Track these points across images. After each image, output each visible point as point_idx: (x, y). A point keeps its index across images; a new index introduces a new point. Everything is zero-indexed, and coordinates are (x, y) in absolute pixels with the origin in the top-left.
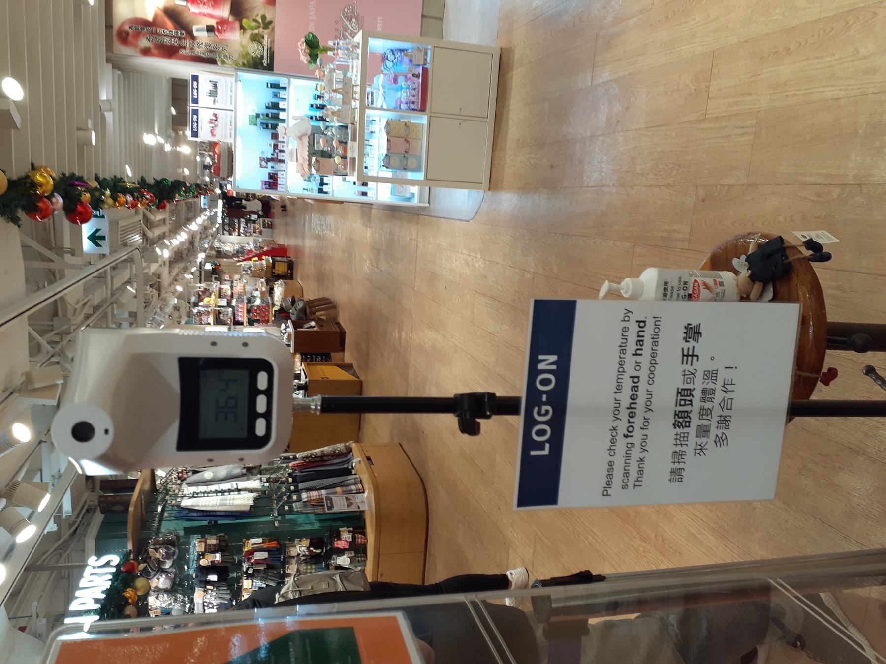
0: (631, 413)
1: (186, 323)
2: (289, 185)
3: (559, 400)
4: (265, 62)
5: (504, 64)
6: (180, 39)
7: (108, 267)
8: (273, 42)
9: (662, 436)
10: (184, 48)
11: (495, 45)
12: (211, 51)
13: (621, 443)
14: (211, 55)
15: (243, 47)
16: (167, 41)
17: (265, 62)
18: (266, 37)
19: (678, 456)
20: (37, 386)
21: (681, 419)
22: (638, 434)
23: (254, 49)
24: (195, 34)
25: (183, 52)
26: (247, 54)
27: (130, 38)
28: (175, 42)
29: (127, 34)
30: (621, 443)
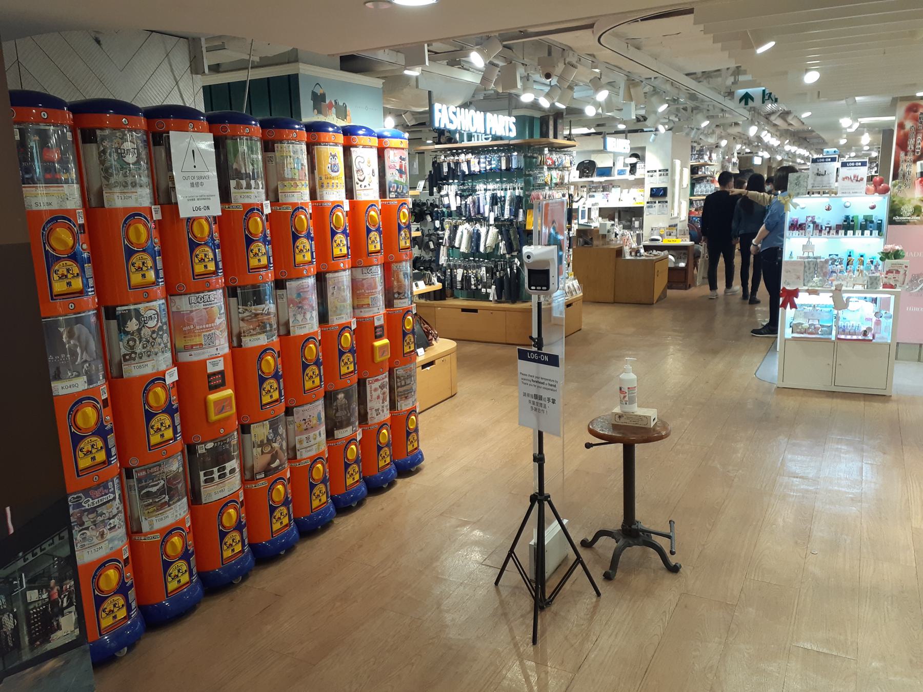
0: (538, 382)
1: (220, 477)
3: (539, 361)
4: (897, 218)
5: (883, 398)
6: (914, 151)
8: (915, 223)
9: (533, 391)
10: (906, 155)
11: (894, 393)
12: (904, 176)
13: (530, 378)
14: (901, 175)
15: (909, 200)
16: (911, 142)
17: (897, 218)
18: (919, 218)
19: (528, 395)
20: (632, 91)
21: (536, 397)
22: (532, 383)
23: (907, 209)
24: (919, 163)
25: (902, 154)
26: (903, 204)
27: (912, 114)
28: (910, 147)
29: (916, 111)
30: (530, 378)
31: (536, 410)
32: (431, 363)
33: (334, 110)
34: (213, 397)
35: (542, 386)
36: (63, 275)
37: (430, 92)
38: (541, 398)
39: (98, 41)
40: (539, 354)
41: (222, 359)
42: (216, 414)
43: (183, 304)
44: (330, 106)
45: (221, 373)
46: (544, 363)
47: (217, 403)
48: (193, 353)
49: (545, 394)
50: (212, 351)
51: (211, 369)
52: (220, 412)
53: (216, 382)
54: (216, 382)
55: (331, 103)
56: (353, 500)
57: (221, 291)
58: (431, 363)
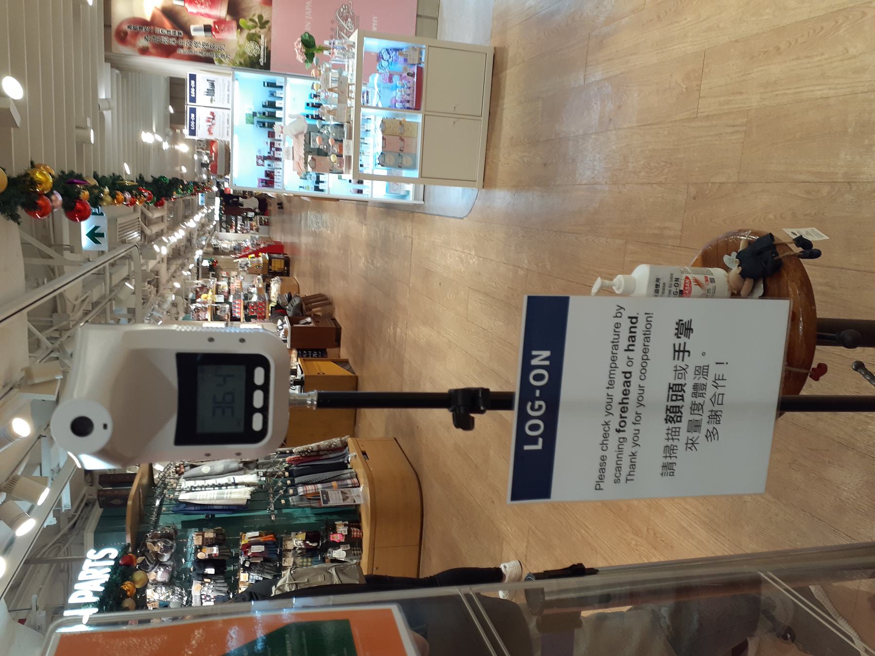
0: (623, 408)
1: (184, 319)
3: (552, 395)
4: (262, 61)
5: (497, 64)
6: (178, 38)
8: (269, 42)
9: (654, 430)
10: (182, 47)
11: (489, 45)
12: (208, 51)
13: (614, 437)
14: (208, 55)
15: (240, 46)
16: (165, 41)
17: (262, 61)
18: (262, 37)
19: (670, 451)
21: (673, 414)
22: (630, 429)
23: (251, 49)
24: (193, 33)
25: (181, 51)
26: (244, 53)
27: (129, 38)
28: (172, 42)
29: (126, 33)
30: (614, 437)
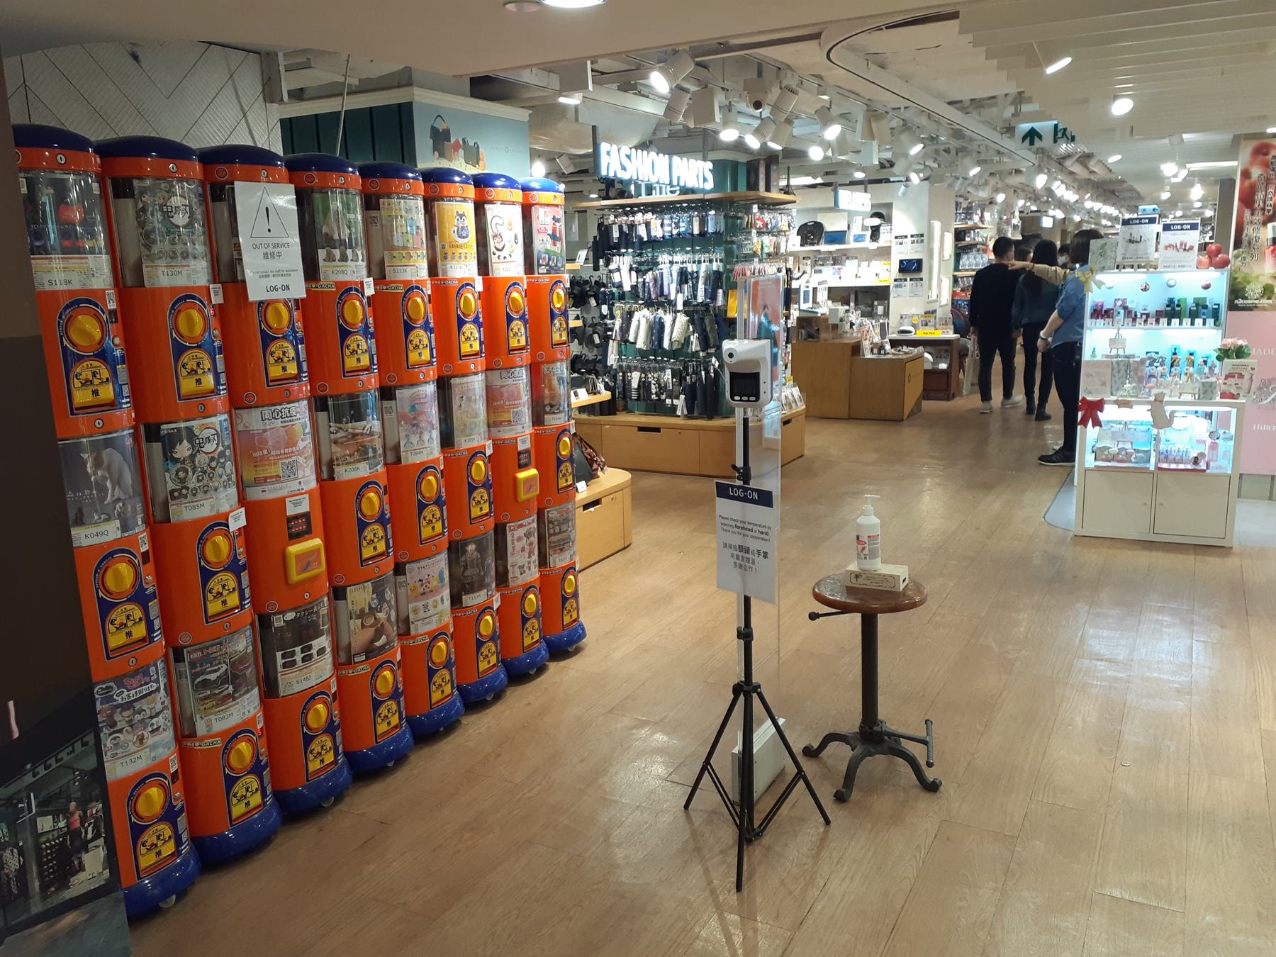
0: (744, 528)
1: (304, 660)
2: (1095, 331)
3: (745, 499)
4: (1240, 302)
5: (1221, 550)
6: (1263, 209)
7: (37, 907)
8: (1264, 309)
9: (737, 540)
10: (1252, 214)
11: (1235, 544)
12: (1250, 243)
13: (733, 523)
14: (1245, 243)
15: (1257, 277)
16: (1260, 196)
17: (1240, 302)
18: (1270, 301)
19: (730, 546)
21: (741, 548)
22: (736, 530)
23: (1254, 289)
24: (1270, 225)
25: (1247, 213)
26: (1249, 283)
27: (1261, 157)
28: (1258, 203)
29: (1266, 154)
30: (733, 523)
31: (741, 566)
32: (596, 502)
33: (461, 152)
34: (295, 549)
35: (750, 533)
36: (87, 380)
37: (594, 128)
38: (747, 550)
39: (135, 57)
40: (745, 490)
41: (307, 496)
42: (299, 573)
43: (253, 420)
44: (456, 147)
45: (306, 516)
46: (753, 501)
47: (299, 557)
48: (266, 488)
49: (754, 545)
50: (294, 486)
51: (291, 511)
52: (305, 570)
53: (299, 528)
54: (299, 528)
55: (457, 142)
56: (487, 691)
57: (305, 402)
58: (596, 502)
